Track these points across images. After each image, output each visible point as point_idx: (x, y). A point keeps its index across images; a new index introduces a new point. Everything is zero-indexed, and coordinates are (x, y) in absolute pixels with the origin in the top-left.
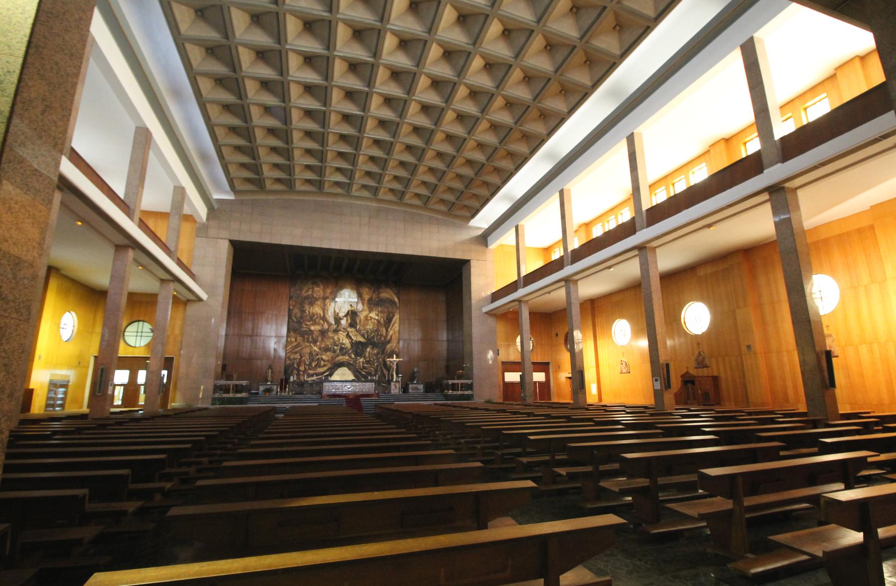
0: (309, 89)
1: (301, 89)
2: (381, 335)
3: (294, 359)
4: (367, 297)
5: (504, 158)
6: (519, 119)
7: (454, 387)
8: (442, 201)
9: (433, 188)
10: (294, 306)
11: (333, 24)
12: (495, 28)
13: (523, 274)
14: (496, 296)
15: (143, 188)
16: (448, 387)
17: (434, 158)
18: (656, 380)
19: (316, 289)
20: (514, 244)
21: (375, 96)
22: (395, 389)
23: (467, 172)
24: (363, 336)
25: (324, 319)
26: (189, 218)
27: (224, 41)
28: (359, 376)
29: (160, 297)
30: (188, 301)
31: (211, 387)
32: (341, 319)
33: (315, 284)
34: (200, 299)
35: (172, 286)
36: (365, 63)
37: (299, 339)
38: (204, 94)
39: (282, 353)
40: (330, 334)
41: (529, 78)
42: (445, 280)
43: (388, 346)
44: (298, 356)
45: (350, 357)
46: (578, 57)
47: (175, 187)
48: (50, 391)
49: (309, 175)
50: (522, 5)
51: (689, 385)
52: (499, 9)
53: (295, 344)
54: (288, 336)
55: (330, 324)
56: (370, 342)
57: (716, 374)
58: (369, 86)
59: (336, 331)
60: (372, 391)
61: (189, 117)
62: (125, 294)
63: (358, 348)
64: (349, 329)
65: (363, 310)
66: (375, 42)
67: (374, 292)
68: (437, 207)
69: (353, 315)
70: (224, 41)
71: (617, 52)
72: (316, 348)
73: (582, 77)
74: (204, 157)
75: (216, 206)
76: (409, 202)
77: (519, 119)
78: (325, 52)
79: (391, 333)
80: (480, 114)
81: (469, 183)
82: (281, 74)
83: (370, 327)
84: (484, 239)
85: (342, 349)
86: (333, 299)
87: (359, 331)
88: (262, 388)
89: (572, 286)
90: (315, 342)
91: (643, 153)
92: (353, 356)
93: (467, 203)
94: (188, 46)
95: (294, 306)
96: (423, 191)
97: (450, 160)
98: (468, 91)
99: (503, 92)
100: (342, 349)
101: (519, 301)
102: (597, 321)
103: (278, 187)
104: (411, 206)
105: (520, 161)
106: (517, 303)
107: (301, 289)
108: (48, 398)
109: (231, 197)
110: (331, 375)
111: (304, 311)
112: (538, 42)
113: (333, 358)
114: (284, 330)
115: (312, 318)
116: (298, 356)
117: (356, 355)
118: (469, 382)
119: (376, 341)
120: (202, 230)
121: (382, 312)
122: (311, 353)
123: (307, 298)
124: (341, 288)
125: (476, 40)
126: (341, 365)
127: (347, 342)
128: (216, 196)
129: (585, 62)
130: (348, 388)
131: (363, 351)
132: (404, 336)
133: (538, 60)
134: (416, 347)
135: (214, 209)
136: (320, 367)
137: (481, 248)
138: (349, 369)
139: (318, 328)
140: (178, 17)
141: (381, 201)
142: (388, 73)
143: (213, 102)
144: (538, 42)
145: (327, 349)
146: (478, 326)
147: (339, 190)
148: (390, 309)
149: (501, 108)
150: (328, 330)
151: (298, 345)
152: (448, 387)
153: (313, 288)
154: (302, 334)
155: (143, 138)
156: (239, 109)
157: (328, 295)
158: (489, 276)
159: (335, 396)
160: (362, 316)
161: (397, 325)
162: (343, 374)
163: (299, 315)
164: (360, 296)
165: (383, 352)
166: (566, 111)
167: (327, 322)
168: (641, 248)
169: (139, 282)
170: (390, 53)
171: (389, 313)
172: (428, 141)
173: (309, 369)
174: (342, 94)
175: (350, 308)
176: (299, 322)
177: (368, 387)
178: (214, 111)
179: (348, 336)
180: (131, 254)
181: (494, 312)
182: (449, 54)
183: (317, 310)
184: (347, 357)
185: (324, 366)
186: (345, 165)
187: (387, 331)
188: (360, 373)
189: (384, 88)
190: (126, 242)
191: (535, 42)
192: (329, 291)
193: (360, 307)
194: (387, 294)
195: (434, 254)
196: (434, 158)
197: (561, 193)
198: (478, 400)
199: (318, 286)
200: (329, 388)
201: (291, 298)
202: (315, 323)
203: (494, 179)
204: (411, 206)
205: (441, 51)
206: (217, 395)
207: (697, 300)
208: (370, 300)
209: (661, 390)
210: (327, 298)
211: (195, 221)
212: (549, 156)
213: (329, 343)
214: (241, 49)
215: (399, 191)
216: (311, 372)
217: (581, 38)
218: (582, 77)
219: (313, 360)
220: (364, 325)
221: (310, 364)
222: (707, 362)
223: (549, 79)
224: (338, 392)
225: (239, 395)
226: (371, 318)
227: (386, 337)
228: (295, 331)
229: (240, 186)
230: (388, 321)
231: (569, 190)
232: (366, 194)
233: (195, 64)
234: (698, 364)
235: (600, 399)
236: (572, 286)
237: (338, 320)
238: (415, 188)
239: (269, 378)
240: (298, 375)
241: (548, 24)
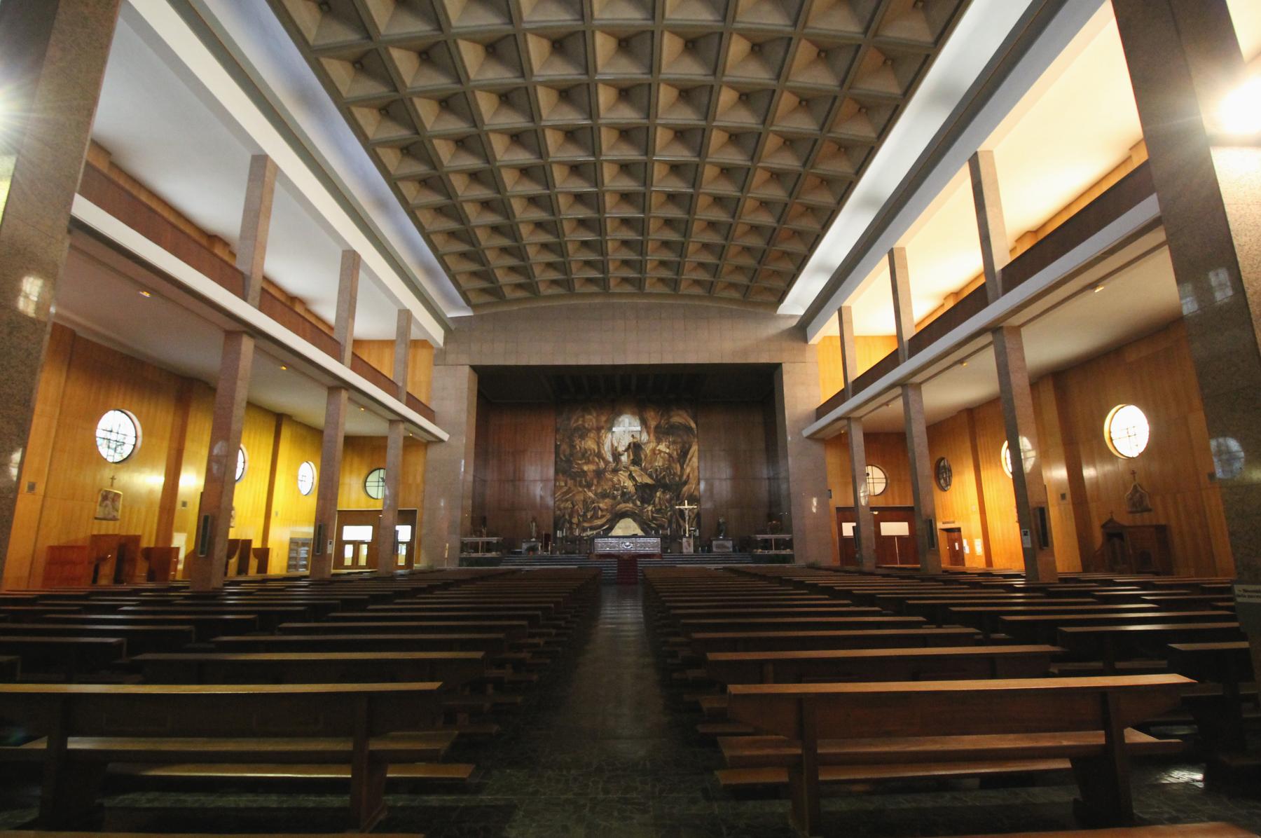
0: (525, 171)
1: (516, 173)
2: (675, 474)
4: (653, 424)
5: (802, 215)
6: (807, 159)
7: (766, 544)
8: (732, 285)
9: (715, 270)
10: (562, 441)
11: (531, 90)
12: (737, 48)
13: (851, 379)
14: (822, 411)
15: (353, 318)
16: (757, 544)
17: (703, 230)
18: (1026, 534)
19: (588, 417)
20: (838, 334)
21: (605, 165)
22: (688, 546)
23: (755, 242)
24: (650, 476)
25: (600, 455)
26: (424, 344)
27: (416, 138)
28: (647, 528)
29: (389, 441)
30: (429, 442)
31: (458, 545)
32: (621, 455)
33: (586, 410)
34: (441, 441)
35: (402, 426)
36: (582, 128)
37: (570, 482)
38: (410, 201)
39: (550, 502)
40: (608, 475)
41: (807, 101)
42: (749, 394)
43: (685, 489)
44: (569, 505)
45: (635, 504)
46: (871, 57)
47: (400, 311)
48: (291, 550)
49: (554, 275)
50: (767, 8)
51: (1116, 541)
52: (734, 20)
53: (565, 489)
54: (556, 480)
55: (607, 463)
56: (660, 484)
57: (1163, 522)
58: (594, 154)
59: (615, 471)
60: (657, 551)
61: (398, 228)
62: (341, 440)
63: (645, 492)
64: (632, 468)
65: (649, 442)
66: (586, 99)
68: (725, 294)
69: (635, 447)
70: (416, 138)
71: (927, 37)
72: (591, 494)
73: (886, 85)
74: (429, 271)
75: (453, 327)
76: (686, 292)
77: (807, 159)
78: (530, 125)
79: (688, 470)
80: (749, 163)
81: (762, 257)
82: (488, 162)
83: (659, 463)
84: (801, 330)
85: (623, 494)
86: (610, 429)
87: (644, 470)
88: (525, 546)
89: (911, 393)
90: (589, 486)
91: (995, 181)
93: (765, 284)
94: (380, 151)
95: (562, 441)
96: (703, 276)
97: (727, 231)
98: (726, 136)
99: (774, 128)
100: (623, 494)
101: (846, 417)
102: (981, 442)
103: (520, 294)
104: (691, 297)
105: (827, 217)
106: (845, 422)
107: (569, 419)
108: (290, 558)
109: (468, 313)
110: (611, 529)
111: (574, 447)
112: (804, 52)
113: (613, 507)
114: (551, 472)
115: (585, 455)
116: (569, 505)
117: (643, 502)
118: (787, 537)
119: (668, 484)
120: (440, 357)
121: (674, 443)
123: (577, 429)
124: (620, 414)
125: (716, 68)
126: (623, 515)
127: (629, 484)
128: (451, 314)
129: (885, 62)
130: (628, 546)
131: (652, 496)
132: (708, 477)
133: (810, 75)
134: (724, 488)
135: (452, 330)
137: (798, 345)
139: (592, 467)
140: (362, 122)
141: (650, 295)
142: (615, 134)
143: (421, 207)
144: (804, 52)
145: (604, 495)
146: (797, 460)
147: (594, 289)
148: (685, 438)
149: (779, 149)
150: (604, 470)
151: (569, 491)
152: (757, 544)
154: (573, 476)
155: (351, 262)
156: (450, 210)
157: (602, 424)
158: (810, 386)
159: (609, 556)
160: (648, 449)
161: (695, 460)
162: (627, 527)
163: (568, 452)
164: (644, 423)
165: (678, 497)
166: (873, 135)
167: (604, 459)
168: (994, 328)
169: (357, 423)
170: (610, 109)
171: (684, 443)
172: (690, 210)
174: (566, 170)
175: (631, 440)
176: (569, 461)
177: (652, 544)
178: (426, 217)
179: (631, 477)
180: (344, 395)
181: (818, 436)
182: (686, 93)
183: (590, 444)
185: (603, 516)
186: (592, 257)
187: (682, 468)
188: (649, 526)
189: (615, 153)
190: (337, 383)
191: (798, 55)
192: (603, 419)
193: (645, 437)
194: (680, 418)
195: (727, 360)
196: (703, 230)
197: (891, 254)
198: (800, 562)
199: (590, 414)
200: (603, 545)
201: (557, 431)
203: (797, 247)
204: (691, 297)
205: (675, 93)
206: (465, 555)
207: (1128, 402)
208: (657, 427)
209: (1033, 548)
211: (431, 347)
212: (867, 202)
213: (607, 486)
214: (436, 142)
215: (671, 280)
216: (586, 525)
217: (866, 31)
218: (886, 85)
219: (587, 510)
221: (585, 515)
222: (1147, 502)
223: (835, 98)
224: (614, 551)
225: (488, 555)
226: (660, 451)
228: (565, 472)
229: (475, 299)
230: (684, 454)
231: (903, 249)
232: (628, 289)
233: (391, 169)
234: (1134, 505)
235: (989, 561)
236: (911, 393)
237: (616, 455)
238: (689, 275)
239: (534, 534)
240: (571, 528)
241: (810, 24)
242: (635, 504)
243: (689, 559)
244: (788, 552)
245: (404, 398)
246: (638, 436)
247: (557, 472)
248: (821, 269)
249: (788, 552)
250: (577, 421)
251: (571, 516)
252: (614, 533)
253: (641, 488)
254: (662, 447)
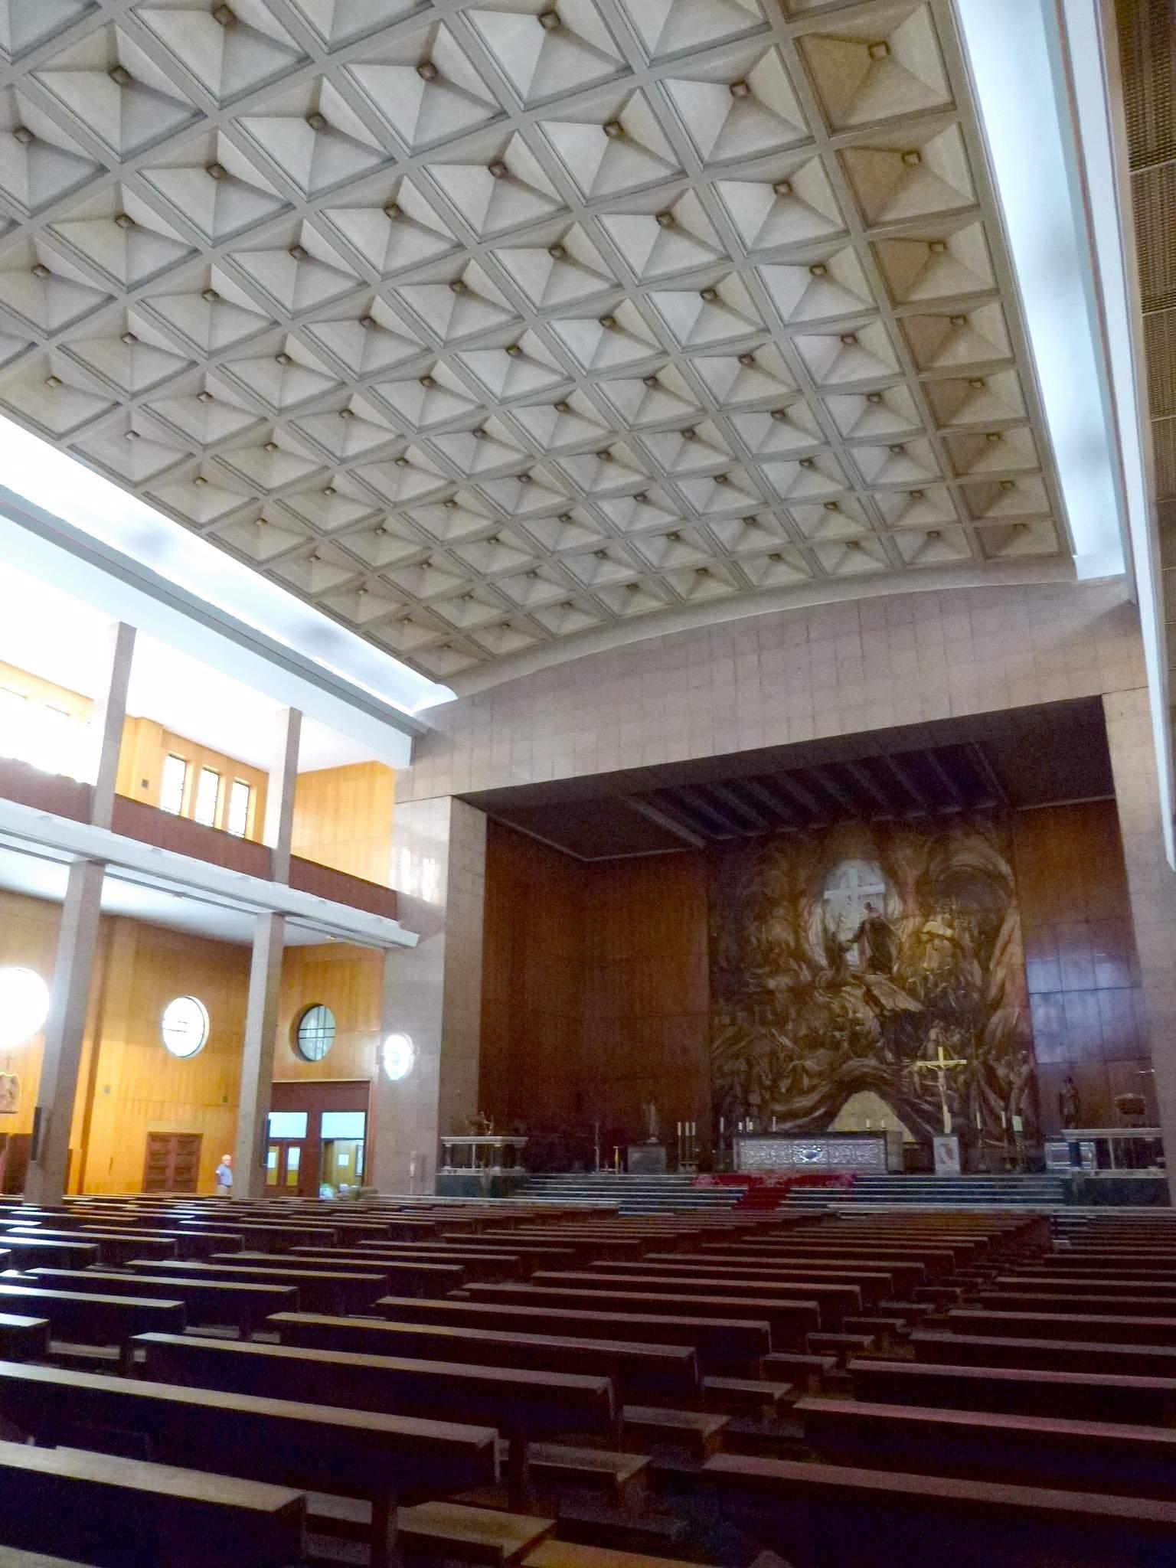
3: (732, 1073)
4: (911, 875)
24: (912, 993)
25: (799, 955)
31: (432, 1153)
40: (820, 997)
43: (996, 1019)
45: (882, 1060)
53: (731, 1031)
54: (714, 1013)
55: (815, 968)
59: (834, 987)
64: (871, 978)
67: (932, 853)
69: (876, 931)
79: (1000, 974)
85: (855, 1038)
87: (899, 980)
92: (889, 1056)
100: (855, 1038)
110: (831, 1115)
115: (771, 957)
116: (742, 1065)
117: (898, 1054)
120: (405, 791)
121: (962, 913)
122: (773, 1055)
127: (866, 1014)
135: (423, 740)
136: (802, 1092)
138: (883, 1096)
145: (814, 1042)
150: (812, 986)
153: (760, 873)
157: (803, 886)
160: (904, 932)
161: (1016, 950)
164: (891, 874)
173: (774, 1099)
179: (870, 999)
183: (779, 931)
184: (872, 1062)
187: (985, 969)
193: (895, 906)
194: (973, 852)
201: (711, 908)
202: (777, 971)
210: (803, 894)
213: (818, 1021)
216: (778, 1108)
219: (778, 1076)
220: (914, 960)
221: (774, 1087)
226: (932, 936)
227: (983, 991)
230: (988, 938)
237: (835, 952)
242: (882, 1060)
243: (945, 1191)
244: (1152, 1172)
245: (283, 868)
246: (879, 905)
247: (713, 997)
249: (1152, 1172)
250: (751, 881)
251: (746, 1091)
252: (838, 1125)
253: (894, 1021)
254: (936, 925)
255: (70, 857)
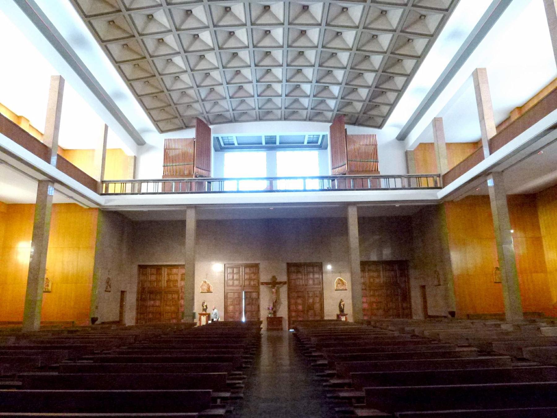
248: (455, 34)
255: (42, 177)
